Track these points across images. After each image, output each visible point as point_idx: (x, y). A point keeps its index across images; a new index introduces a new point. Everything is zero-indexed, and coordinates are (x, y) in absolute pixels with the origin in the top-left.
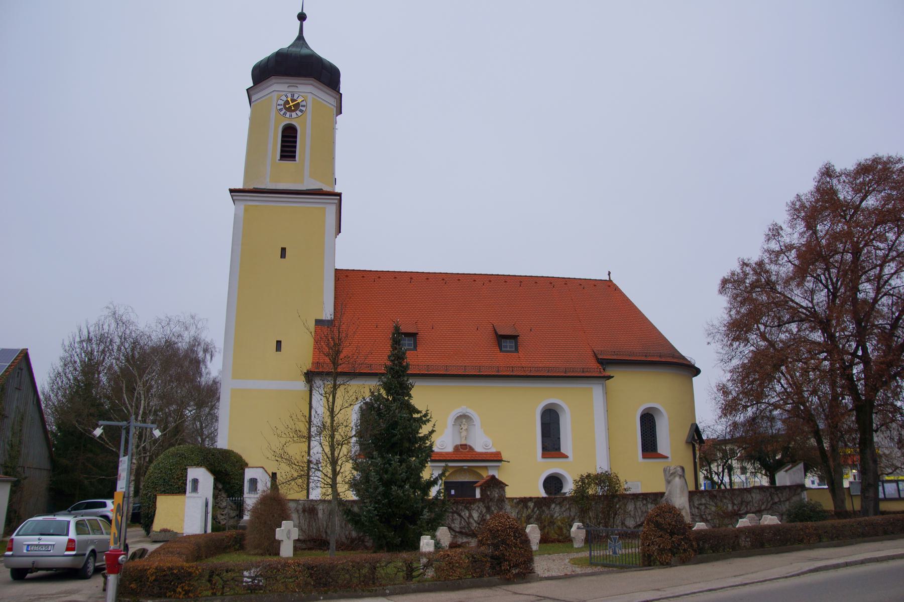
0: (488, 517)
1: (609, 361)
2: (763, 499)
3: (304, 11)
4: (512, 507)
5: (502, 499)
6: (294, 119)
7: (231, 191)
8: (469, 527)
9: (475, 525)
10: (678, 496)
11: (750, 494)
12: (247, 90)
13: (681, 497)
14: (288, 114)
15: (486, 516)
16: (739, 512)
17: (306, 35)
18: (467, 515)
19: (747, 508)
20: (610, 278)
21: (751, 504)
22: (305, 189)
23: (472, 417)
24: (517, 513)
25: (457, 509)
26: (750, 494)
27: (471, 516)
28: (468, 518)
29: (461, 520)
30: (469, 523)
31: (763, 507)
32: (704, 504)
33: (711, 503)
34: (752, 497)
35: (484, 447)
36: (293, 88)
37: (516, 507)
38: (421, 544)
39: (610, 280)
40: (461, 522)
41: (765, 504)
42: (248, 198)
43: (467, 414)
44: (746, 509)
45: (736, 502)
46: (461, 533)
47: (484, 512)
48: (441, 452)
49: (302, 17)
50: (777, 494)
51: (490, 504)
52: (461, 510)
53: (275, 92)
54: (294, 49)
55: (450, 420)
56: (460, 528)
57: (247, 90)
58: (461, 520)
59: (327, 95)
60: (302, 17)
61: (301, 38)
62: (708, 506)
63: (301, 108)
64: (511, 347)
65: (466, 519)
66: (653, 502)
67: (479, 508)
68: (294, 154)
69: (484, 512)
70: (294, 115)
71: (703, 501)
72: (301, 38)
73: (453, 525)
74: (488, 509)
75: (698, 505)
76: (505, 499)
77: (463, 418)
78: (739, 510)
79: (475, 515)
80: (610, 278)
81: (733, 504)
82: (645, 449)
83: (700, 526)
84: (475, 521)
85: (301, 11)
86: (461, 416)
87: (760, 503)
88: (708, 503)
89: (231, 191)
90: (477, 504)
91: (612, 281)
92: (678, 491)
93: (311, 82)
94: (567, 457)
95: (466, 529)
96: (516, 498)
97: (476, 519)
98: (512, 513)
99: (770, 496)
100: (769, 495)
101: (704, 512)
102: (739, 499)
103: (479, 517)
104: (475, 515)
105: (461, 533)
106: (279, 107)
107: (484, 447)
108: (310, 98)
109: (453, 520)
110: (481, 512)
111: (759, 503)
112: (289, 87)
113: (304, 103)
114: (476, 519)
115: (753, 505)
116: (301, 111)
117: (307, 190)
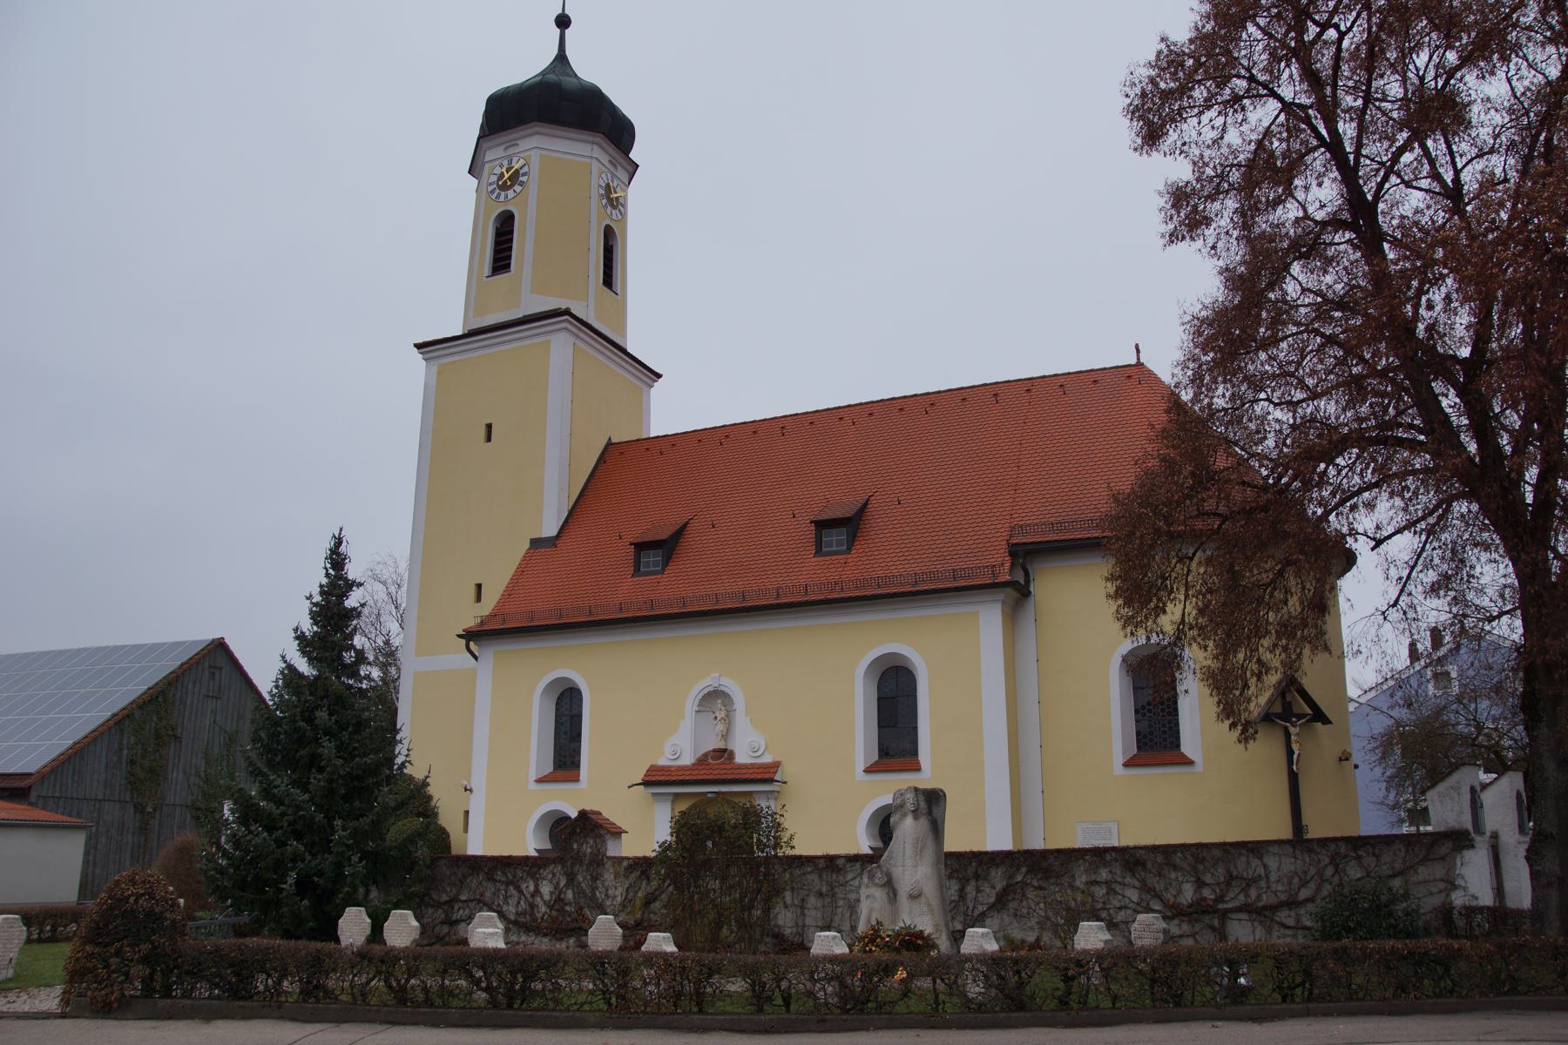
0: (570, 895)
1: (1030, 547)
2: (1305, 873)
3: (566, 12)
4: (616, 875)
5: (598, 860)
6: (510, 201)
7: (419, 346)
8: (532, 914)
9: (544, 909)
10: (909, 862)
11: (1261, 858)
12: (638, 166)
13: (916, 866)
14: (503, 194)
15: (565, 893)
16: (1221, 906)
17: (570, 53)
18: (532, 888)
19: (1247, 896)
20: (1138, 359)
21: (1263, 883)
22: (521, 316)
23: (730, 693)
24: (627, 890)
25: (514, 876)
26: (1261, 858)
27: (537, 892)
28: (533, 896)
29: (520, 899)
30: (532, 906)
31: (1304, 894)
32: (1106, 882)
33: (1129, 880)
34: (1265, 867)
35: (751, 754)
36: (513, 148)
37: (627, 877)
38: (402, 945)
39: (1139, 364)
40: (519, 903)
41: (1312, 885)
42: (596, 345)
43: (722, 688)
44: (1241, 897)
45: (1208, 878)
46: (515, 923)
47: (562, 885)
48: (671, 767)
49: (563, 22)
50: (1359, 858)
51: (576, 869)
52: (522, 878)
53: (536, 150)
54: (552, 77)
55: (691, 704)
56: (517, 913)
57: (638, 166)
58: (520, 899)
59: (578, 143)
60: (563, 22)
61: (561, 58)
62: (1118, 888)
63: (521, 179)
64: (839, 543)
65: (528, 896)
66: (956, 875)
67: (554, 875)
68: (507, 262)
69: (562, 885)
70: (511, 193)
71: (1104, 874)
72: (561, 58)
73: (505, 908)
74: (571, 878)
75: (1087, 883)
76: (605, 860)
77: (715, 698)
78: (1220, 899)
79: (546, 889)
80: (1138, 359)
81: (1200, 884)
82: (1146, 744)
83: (980, 940)
84: (545, 902)
85: (560, 11)
86: (709, 694)
87: (1296, 881)
88: (1119, 879)
89: (419, 346)
90: (552, 867)
91: (1143, 364)
92: (909, 851)
93: (536, 129)
94: (1190, 763)
95: (528, 916)
96: (627, 858)
97: (547, 897)
98: (616, 888)
99: (1333, 861)
100: (1326, 860)
101: (1104, 903)
102: (1221, 871)
103: (551, 893)
104: (546, 889)
105: (515, 923)
106: (490, 188)
107: (751, 754)
108: (535, 156)
109: (506, 898)
110: (558, 883)
111: (1290, 883)
112: (506, 148)
113: (525, 169)
114: (547, 897)
115: (1269, 887)
116: (522, 184)
117: (524, 317)
